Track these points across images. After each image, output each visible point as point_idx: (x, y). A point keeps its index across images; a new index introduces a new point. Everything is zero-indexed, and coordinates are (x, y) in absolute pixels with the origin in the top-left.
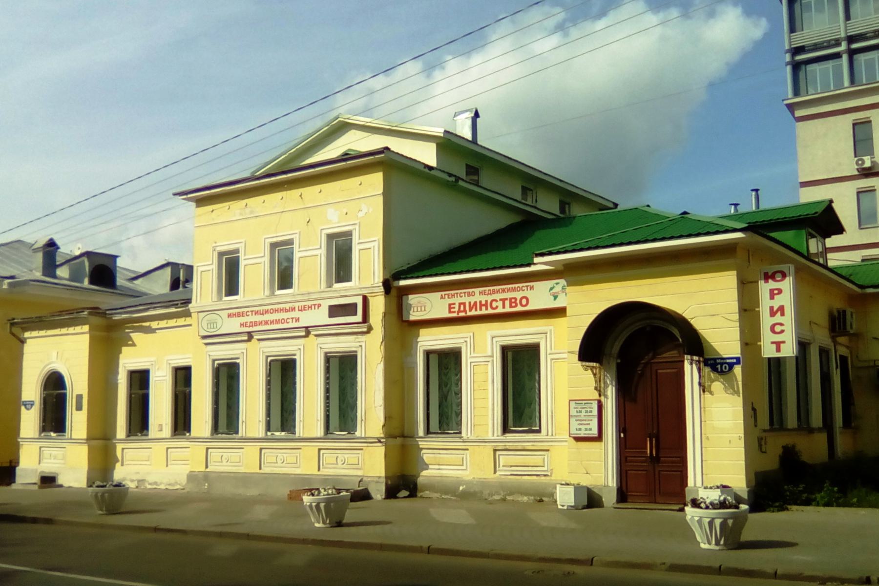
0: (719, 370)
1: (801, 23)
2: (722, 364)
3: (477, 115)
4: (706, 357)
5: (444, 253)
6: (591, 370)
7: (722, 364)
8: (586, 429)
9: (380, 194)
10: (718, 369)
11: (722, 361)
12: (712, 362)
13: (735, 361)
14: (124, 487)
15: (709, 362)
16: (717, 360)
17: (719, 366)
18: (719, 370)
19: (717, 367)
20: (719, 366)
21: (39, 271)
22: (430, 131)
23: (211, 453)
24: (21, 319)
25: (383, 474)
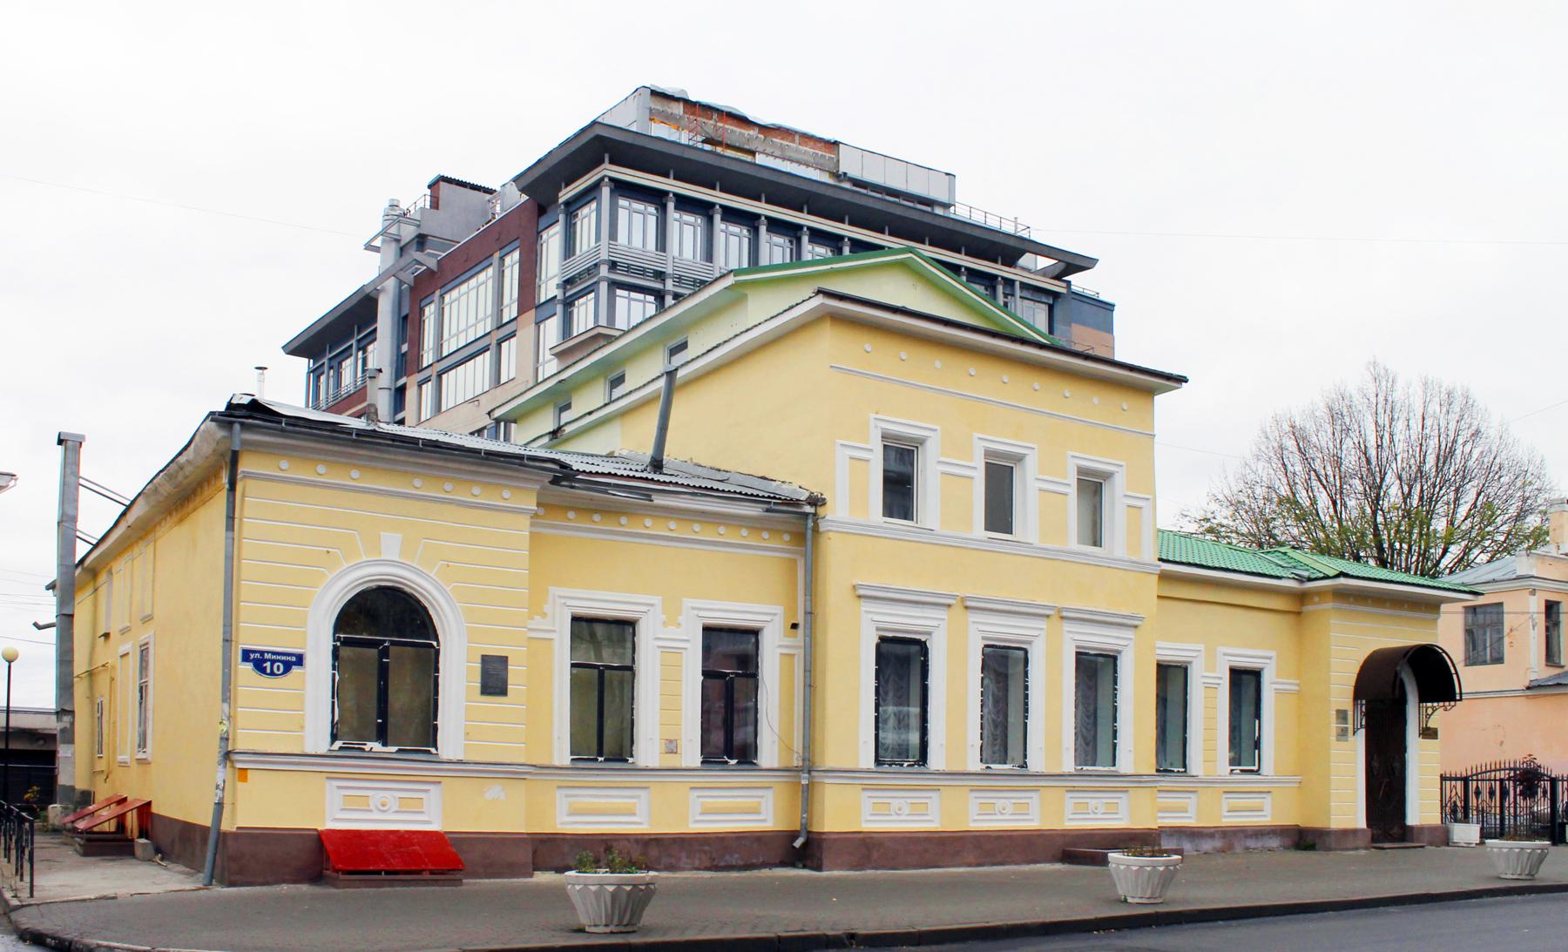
0: (268, 671)
1: (1021, 736)
2: (273, 662)
4: (722, 681)
5: (411, 596)
7: (273, 662)
8: (27, 840)
9: (125, 505)
10: (266, 667)
11: (274, 657)
12: (258, 655)
13: (294, 659)
14: (328, 351)
15: (252, 656)
16: (266, 654)
17: (268, 664)
18: (268, 671)
19: (265, 665)
20: (268, 664)
21: (916, 707)
22: (87, 480)
23: (644, 302)
24: (1173, 771)
25: (826, 830)
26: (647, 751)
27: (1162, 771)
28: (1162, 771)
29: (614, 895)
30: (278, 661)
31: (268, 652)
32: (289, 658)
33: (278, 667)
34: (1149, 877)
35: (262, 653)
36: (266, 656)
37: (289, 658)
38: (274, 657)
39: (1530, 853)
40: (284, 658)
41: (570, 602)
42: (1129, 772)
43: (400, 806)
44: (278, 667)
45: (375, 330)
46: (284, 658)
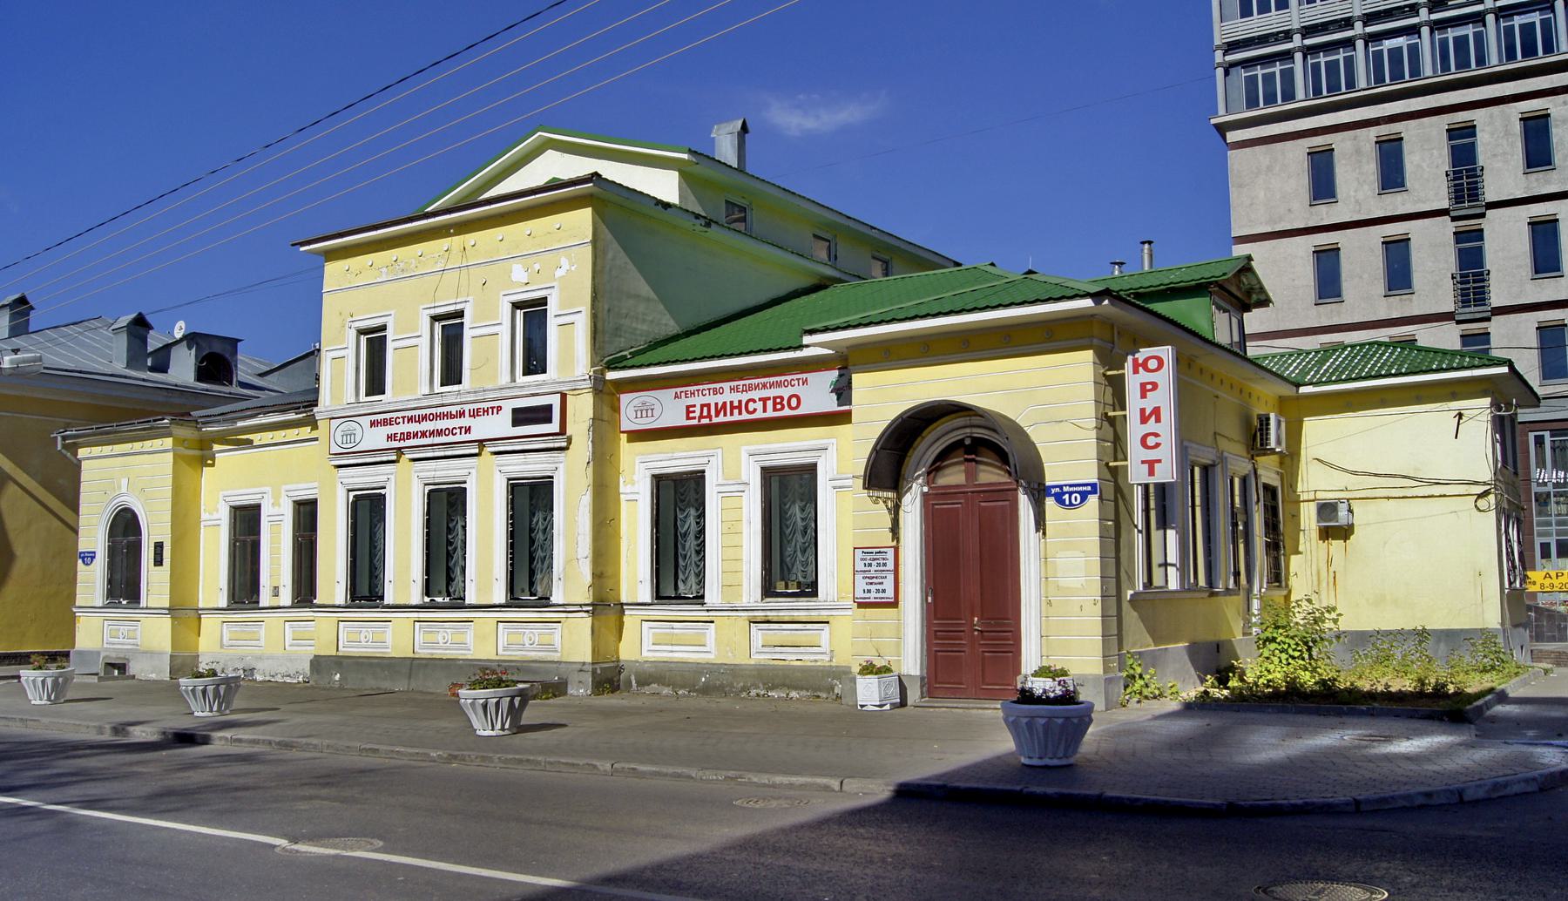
0: (1067, 503)
2: (1071, 494)
3: (744, 128)
6: (884, 502)
7: (1071, 494)
11: (1072, 489)
12: (1058, 490)
13: (1089, 488)
15: (1053, 491)
17: (1066, 496)
18: (1067, 503)
20: (1066, 496)
26: (265, 599)
27: (514, 601)
28: (514, 601)
29: (1046, 727)
30: (1076, 492)
31: (1066, 485)
32: (1085, 488)
33: (1076, 498)
34: (1046, 732)
35: (1061, 487)
36: (1065, 489)
37: (1085, 488)
38: (1072, 489)
39: (1063, 725)
40: (1080, 489)
41: (290, 494)
42: (561, 603)
43: (820, 635)
44: (1076, 498)
45: (726, 217)
46: (1080, 489)
